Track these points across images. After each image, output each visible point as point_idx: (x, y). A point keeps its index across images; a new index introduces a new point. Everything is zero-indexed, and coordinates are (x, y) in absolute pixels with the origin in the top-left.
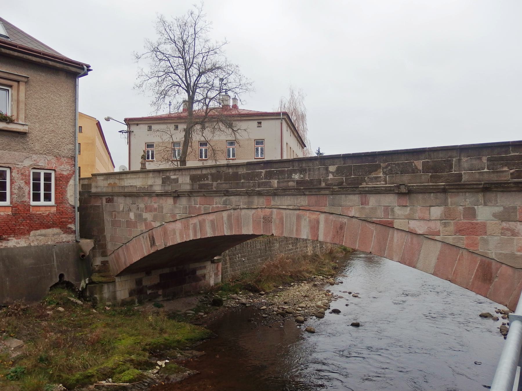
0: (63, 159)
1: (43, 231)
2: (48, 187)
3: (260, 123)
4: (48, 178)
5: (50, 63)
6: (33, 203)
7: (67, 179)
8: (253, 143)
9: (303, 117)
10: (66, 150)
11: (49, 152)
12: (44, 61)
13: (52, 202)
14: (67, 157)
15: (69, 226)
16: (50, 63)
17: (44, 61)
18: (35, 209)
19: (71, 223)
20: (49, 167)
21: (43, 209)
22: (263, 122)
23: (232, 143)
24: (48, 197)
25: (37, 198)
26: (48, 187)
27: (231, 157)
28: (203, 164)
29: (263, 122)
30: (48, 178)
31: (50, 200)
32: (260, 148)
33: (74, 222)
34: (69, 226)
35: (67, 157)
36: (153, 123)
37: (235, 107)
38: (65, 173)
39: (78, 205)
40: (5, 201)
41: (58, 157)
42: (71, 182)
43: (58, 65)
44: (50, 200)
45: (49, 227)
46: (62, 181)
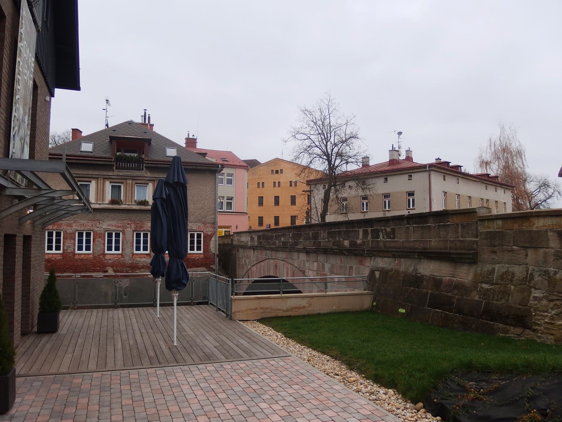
0: (208, 225)
1: (195, 269)
2: (199, 242)
3: (411, 176)
4: (199, 236)
5: (199, 167)
6: (77, 252)
7: (210, 237)
8: (405, 195)
9: (519, 153)
10: (210, 219)
11: (199, 221)
12: (195, 167)
13: (202, 252)
14: (211, 223)
15: (212, 266)
16: (199, 167)
17: (195, 167)
18: (191, 255)
19: (212, 264)
20: (199, 230)
21: (195, 255)
22: (413, 175)
23: (365, 198)
24: (199, 248)
25: (80, 248)
26: (199, 242)
27: (387, 209)
28: (364, 216)
29: (413, 175)
30: (199, 236)
31: (200, 250)
32: (411, 199)
33: (214, 264)
34: (212, 266)
35: (211, 223)
36: (389, 175)
37: (409, 158)
38: (209, 233)
39: (217, 253)
40: (52, 250)
41: (205, 223)
42: (213, 239)
43: (204, 168)
44: (200, 250)
45: (199, 267)
46: (208, 238)
